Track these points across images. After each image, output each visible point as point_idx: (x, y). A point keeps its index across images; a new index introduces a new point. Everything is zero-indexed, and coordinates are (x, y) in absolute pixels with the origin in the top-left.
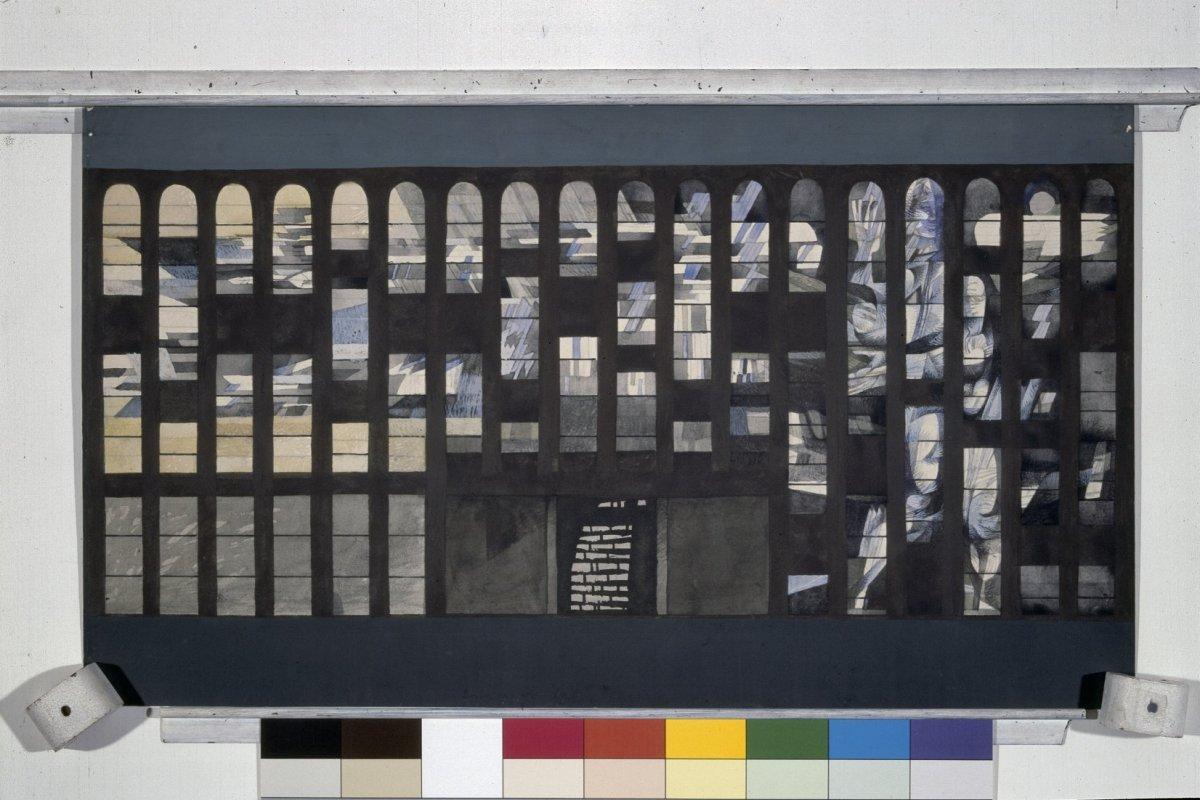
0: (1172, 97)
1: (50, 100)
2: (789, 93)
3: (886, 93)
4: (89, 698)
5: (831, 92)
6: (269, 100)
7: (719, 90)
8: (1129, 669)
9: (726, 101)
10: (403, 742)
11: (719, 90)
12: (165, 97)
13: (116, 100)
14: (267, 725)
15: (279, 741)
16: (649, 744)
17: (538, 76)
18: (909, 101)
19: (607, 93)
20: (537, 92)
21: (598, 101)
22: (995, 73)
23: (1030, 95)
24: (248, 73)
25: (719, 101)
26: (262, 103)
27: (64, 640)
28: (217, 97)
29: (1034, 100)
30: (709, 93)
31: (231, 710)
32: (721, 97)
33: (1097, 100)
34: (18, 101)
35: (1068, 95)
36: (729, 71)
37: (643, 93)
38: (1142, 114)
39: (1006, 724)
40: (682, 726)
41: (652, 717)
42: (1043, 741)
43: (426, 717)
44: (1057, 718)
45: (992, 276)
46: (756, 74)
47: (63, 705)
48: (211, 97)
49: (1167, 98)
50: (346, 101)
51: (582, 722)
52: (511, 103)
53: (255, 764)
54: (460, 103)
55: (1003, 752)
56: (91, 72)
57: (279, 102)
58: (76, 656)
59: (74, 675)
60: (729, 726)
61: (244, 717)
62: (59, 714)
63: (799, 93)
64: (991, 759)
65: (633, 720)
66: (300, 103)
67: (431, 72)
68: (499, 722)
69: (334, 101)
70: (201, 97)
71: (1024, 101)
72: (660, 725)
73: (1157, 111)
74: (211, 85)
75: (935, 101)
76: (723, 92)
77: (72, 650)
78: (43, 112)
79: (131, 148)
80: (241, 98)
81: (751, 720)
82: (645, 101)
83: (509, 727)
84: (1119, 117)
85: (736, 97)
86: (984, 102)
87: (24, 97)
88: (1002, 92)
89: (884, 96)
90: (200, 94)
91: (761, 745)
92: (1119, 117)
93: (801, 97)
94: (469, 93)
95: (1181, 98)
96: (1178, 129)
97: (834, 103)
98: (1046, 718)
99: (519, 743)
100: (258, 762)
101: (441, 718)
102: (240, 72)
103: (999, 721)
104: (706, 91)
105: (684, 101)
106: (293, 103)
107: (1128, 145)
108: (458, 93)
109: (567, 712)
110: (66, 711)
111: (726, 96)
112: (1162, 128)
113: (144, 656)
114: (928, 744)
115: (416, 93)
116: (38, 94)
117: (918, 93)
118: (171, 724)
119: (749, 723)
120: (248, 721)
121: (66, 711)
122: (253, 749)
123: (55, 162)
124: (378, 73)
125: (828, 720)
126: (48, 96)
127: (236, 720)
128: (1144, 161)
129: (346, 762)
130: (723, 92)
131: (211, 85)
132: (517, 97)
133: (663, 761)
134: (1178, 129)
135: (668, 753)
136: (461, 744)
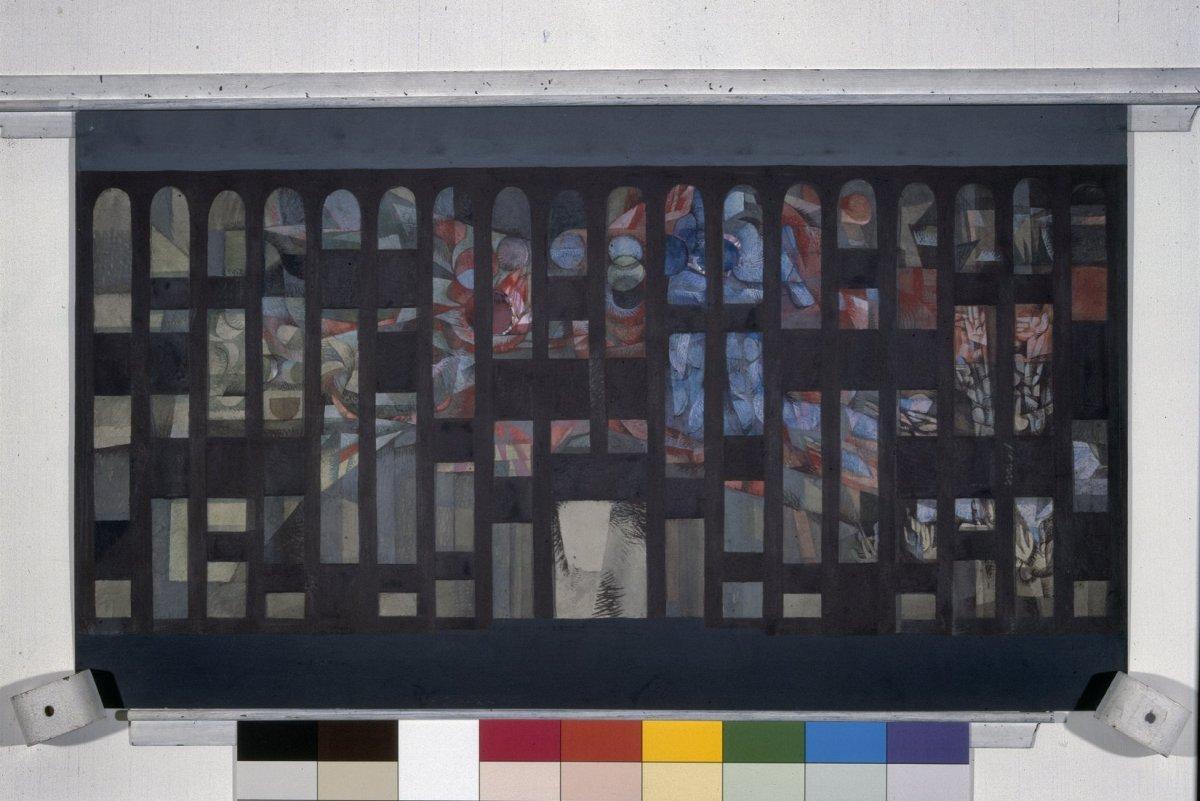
0: (1183, 97)
1: (61, 105)
2: (799, 93)
3: (898, 92)
4: (74, 701)
5: (841, 93)
6: (279, 103)
7: (730, 90)
8: (1125, 671)
9: (737, 102)
10: (380, 744)
11: (730, 90)
12: (175, 101)
13: (125, 104)
14: (244, 727)
15: (255, 744)
16: (626, 747)
17: (549, 77)
18: (920, 101)
19: (618, 93)
20: (548, 93)
21: (609, 102)
22: (1007, 74)
23: (1041, 95)
24: (258, 76)
25: (730, 101)
26: (273, 105)
27: (55, 648)
28: (228, 101)
29: (1045, 100)
30: (720, 93)
31: (185, 713)
32: (732, 97)
33: (1108, 100)
34: (26, 106)
35: (1077, 95)
36: (740, 71)
37: (655, 93)
38: (1134, 115)
39: (983, 726)
40: (660, 728)
41: (620, 719)
42: (1011, 745)
43: (402, 719)
44: (1026, 721)
45: (378, 448)
46: (766, 75)
47: (48, 704)
48: (222, 100)
49: (1178, 98)
50: (357, 103)
51: (559, 723)
52: (524, 103)
53: (477, 766)
54: (471, 104)
55: (978, 755)
56: (101, 77)
57: (290, 105)
58: (68, 663)
59: (66, 678)
60: (705, 728)
61: (214, 720)
62: (42, 713)
63: (810, 93)
64: (967, 763)
65: (600, 721)
66: (309, 105)
67: (440, 73)
68: (476, 723)
69: (345, 104)
70: (211, 100)
71: (1036, 101)
72: (636, 728)
73: (1168, 110)
74: (221, 89)
75: (946, 101)
76: (734, 92)
77: (64, 658)
78: (53, 116)
79: (132, 163)
80: (251, 102)
81: (729, 722)
82: (655, 102)
83: (487, 732)
84: (1109, 121)
85: (747, 97)
86: (995, 102)
87: (34, 102)
88: (1013, 92)
89: (896, 96)
90: (210, 97)
91: (738, 748)
92: (1109, 121)
93: (812, 98)
94: (479, 94)
95: (1192, 98)
96: (1189, 130)
97: (846, 103)
98: (1016, 722)
99: (496, 746)
100: (234, 767)
101: (409, 719)
102: (250, 75)
103: (973, 724)
104: (718, 92)
105: (695, 101)
106: (302, 106)
107: (1122, 148)
108: (469, 94)
109: (509, 713)
110: (49, 711)
111: (737, 97)
112: (1173, 128)
113: (133, 665)
114: (904, 748)
115: (426, 95)
116: (48, 99)
117: (929, 93)
118: (139, 727)
119: (725, 724)
120: (225, 723)
121: (49, 711)
122: (230, 751)
123: (47, 174)
124: (388, 75)
125: (805, 723)
126: (58, 101)
127: (205, 722)
128: (1136, 173)
129: (569, 767)
130: (734, 92)
131: (221, 89)
132: (528, 98)
133: (721, 760)
134: (1189, 130)
135: (645, 756)
136: (438, 746)
